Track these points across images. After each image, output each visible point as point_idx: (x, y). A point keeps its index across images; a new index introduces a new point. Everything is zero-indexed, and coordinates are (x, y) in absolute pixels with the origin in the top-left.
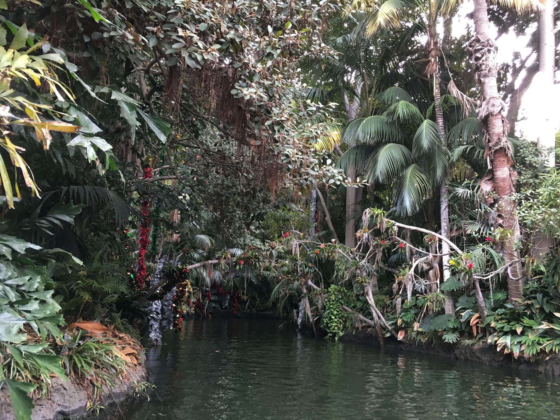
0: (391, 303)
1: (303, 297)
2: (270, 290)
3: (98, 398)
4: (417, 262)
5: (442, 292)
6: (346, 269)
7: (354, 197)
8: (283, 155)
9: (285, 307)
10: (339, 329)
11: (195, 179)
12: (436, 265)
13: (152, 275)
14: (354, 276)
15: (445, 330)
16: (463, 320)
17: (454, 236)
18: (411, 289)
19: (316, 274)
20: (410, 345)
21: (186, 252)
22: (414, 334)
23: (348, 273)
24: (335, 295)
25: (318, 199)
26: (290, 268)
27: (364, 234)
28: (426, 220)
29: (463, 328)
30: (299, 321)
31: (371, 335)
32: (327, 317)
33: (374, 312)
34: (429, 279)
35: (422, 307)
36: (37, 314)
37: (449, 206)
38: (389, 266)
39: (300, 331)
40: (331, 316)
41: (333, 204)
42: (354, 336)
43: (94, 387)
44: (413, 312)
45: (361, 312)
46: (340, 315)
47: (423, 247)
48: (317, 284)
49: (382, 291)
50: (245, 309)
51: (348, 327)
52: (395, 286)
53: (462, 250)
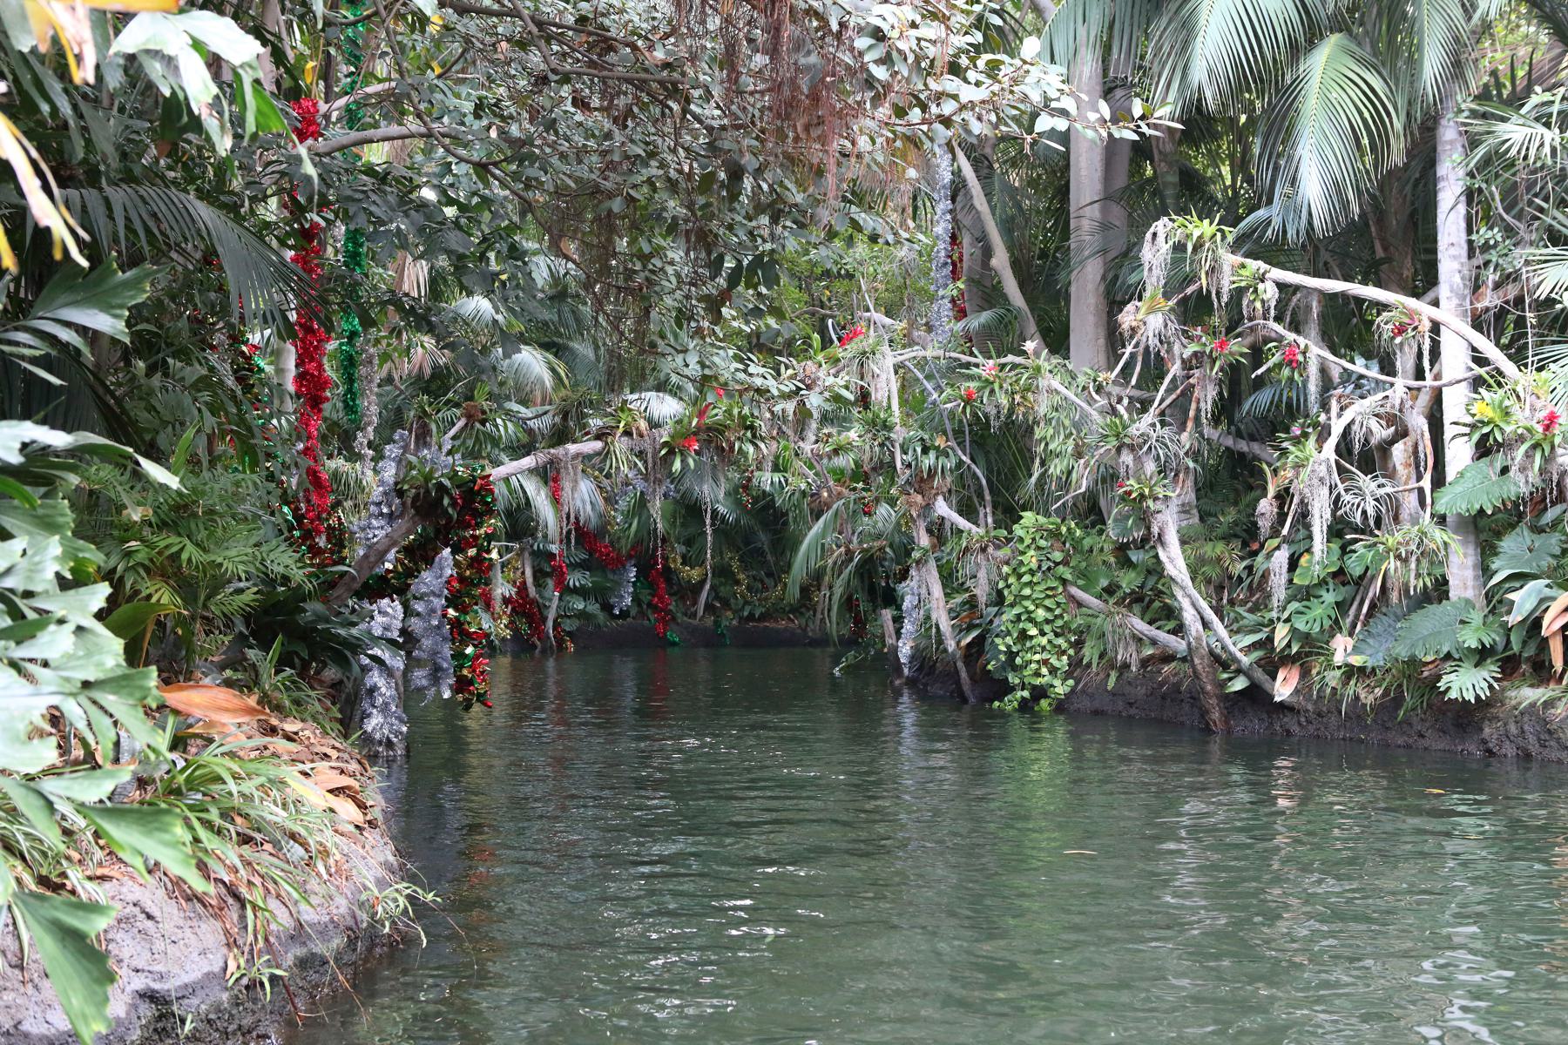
0: (1249, 568)
1: (918, 562)
2: (785, 543)
3: (261, 943)
4: (1348, 415)
5: (1441, 520)
6: (1078, 455)
7: (1098, 174)
8: (860, 30)
9: (849, 603)
10: (1053, 671)
11: (493, 134)
12: (1418, 422)
13: (348, 504)
14: (1109, 477)
15: (1448, 657)
16: (1514, 618)
17: (1487, 309)
18: (1328, 515)
19: (962, 474)
20: (1319, 715)
21: (476, 417)
22: (1333, 678)
23: (1086, 465)
24: (1039, 548)
25: (958, 188)
26: (866, 457)
27: (1148, 319)
28: (1380, 253)
29: (1516, 647)
30: (905, 650)
31: (1176, 688)
32: (1009, 633)
33: (1185, 604)
34: (1391, 475)
35: (1362, 577)
36: (73, 668)
37: (1470, 195)
38: (1239, 435)
39: (911, 682)
40: (1029, 626)
41: (1018, 206)
42: (1113, 694)
43: (243, 907)
44: (1330, 597)
45: (1137, 608)
46: (1059, 623)
47: (1368, 356)
48: (968, 511)
49: (1212, 528)
50: (694, 615)
51: (1089, 665)
52: (1266, 506)
53: (1518, 357)
